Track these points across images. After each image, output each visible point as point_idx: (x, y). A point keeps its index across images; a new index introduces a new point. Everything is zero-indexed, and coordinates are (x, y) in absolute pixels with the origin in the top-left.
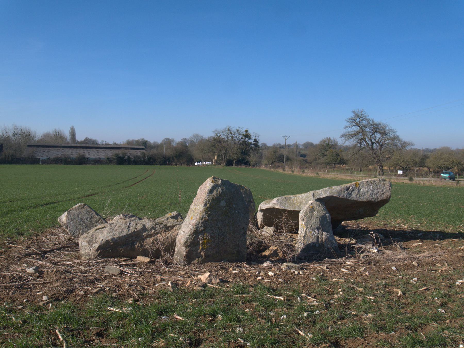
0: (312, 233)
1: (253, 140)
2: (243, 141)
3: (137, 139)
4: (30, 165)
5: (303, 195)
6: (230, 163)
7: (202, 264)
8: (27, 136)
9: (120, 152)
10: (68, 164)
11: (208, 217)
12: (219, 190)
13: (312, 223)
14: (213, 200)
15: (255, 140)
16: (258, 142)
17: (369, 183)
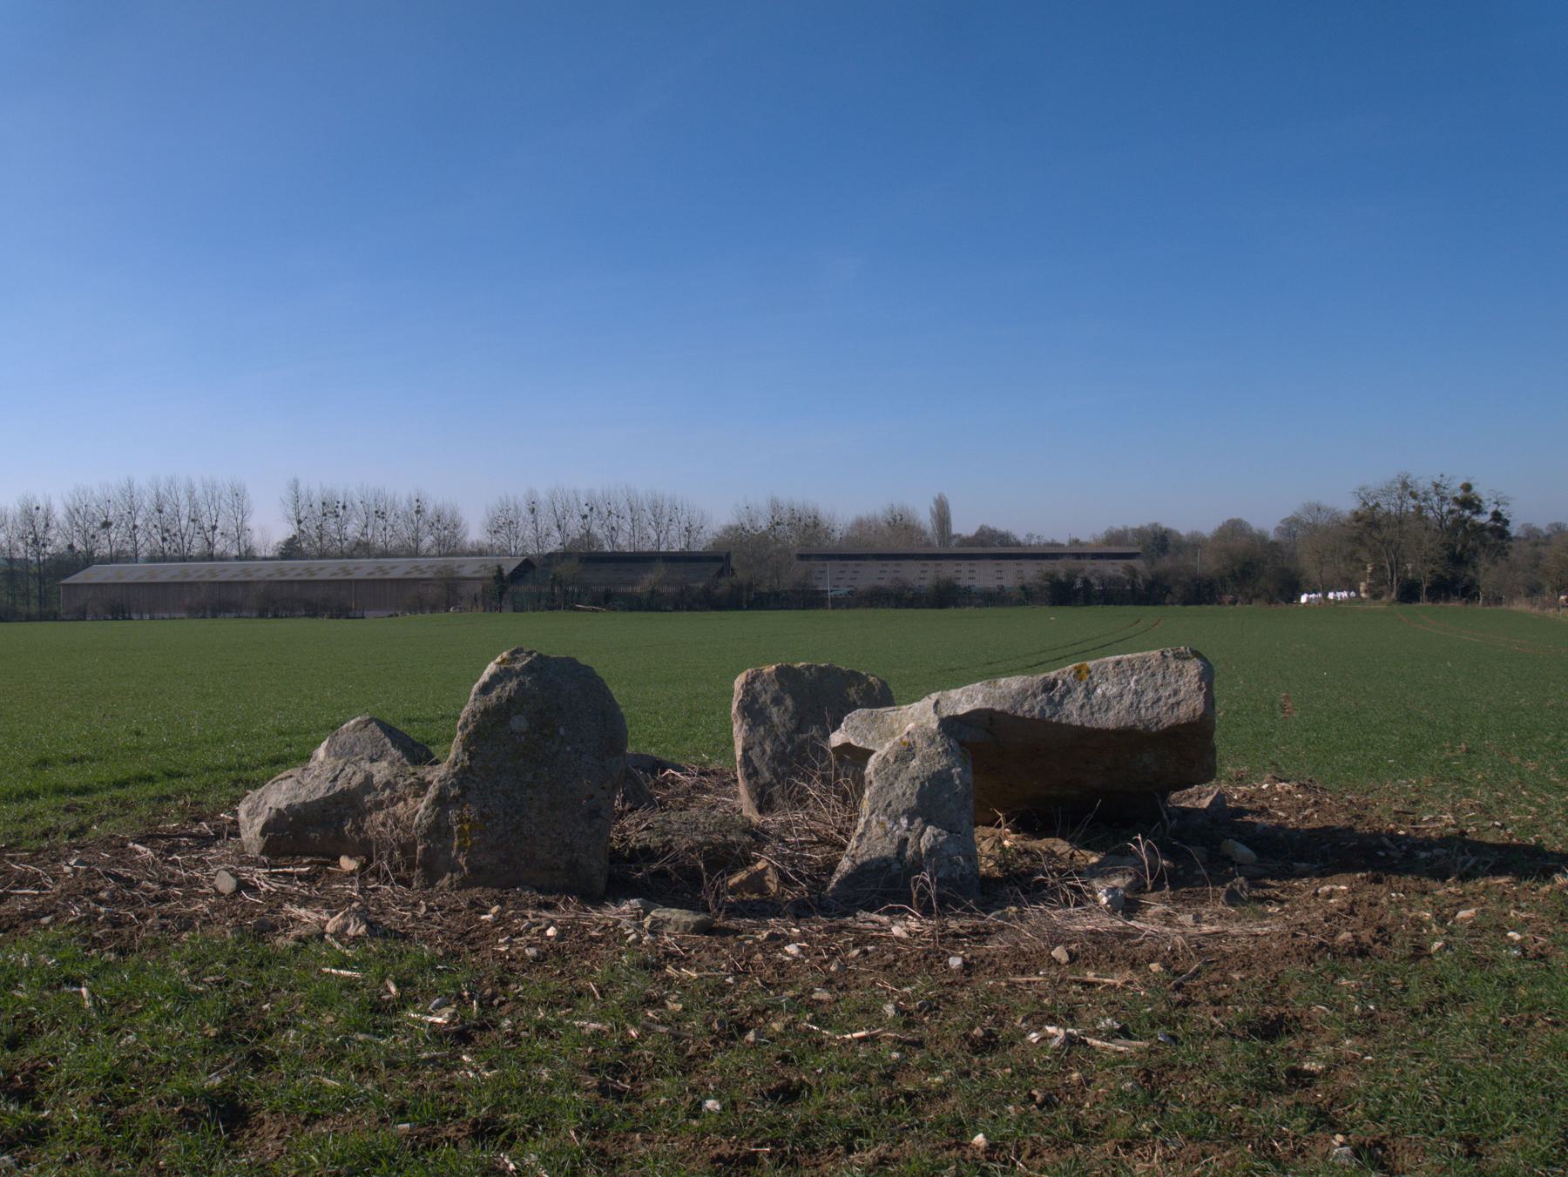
0: (889, 826)
1: (1489, 517)
2: (1455, 521)
3: (1137, 526)
4: (802, 613)
5: (916, 704)
6: (1409, 593)
7: (459, 889)
8: (811, 527)
9: (1060, 568)
10: (908, 606)
11: (470, 759)
12: (512, 685)
13: (892, 795)
14: (486, 712)
15: (1497, 516)
16: (1507, 522)
17: (1125, 665)
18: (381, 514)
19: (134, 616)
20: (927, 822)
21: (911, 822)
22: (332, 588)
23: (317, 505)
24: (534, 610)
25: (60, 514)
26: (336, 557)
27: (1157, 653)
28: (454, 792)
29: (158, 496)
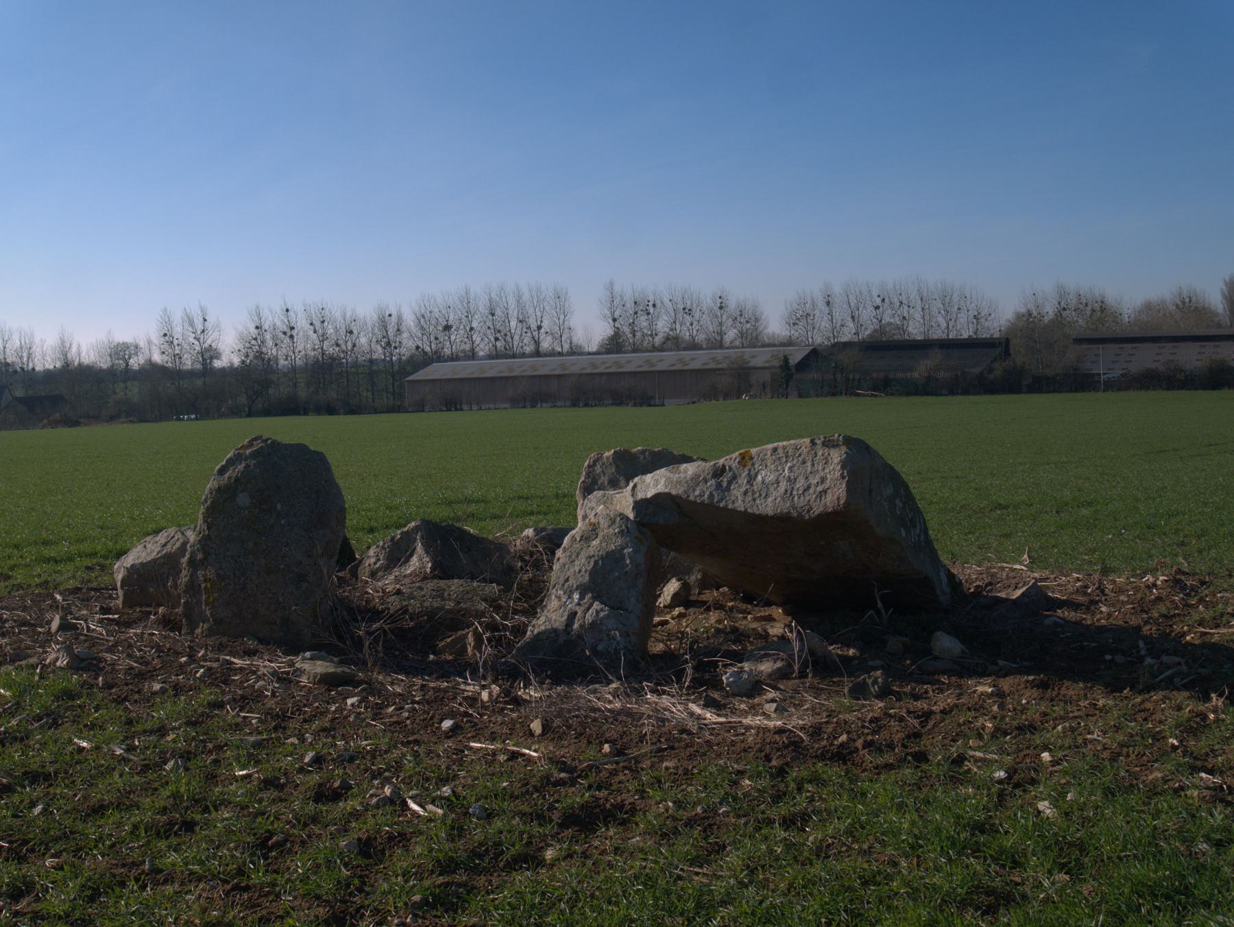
4: (1071, 395)
8: (1102, 311)
11: (209, 529)
12: (241, 467)
14: (219, 490)
18: (688, 311)
19: (465, 407)
20: (595, 598)
21: (582, 598)
22: (652, 379)
23: (630, 305)
24: (817, 396)
25: (409, 320)
26: (647, 351)
27: (807, 441)
28: (200, 556)
29: (490, 300)
